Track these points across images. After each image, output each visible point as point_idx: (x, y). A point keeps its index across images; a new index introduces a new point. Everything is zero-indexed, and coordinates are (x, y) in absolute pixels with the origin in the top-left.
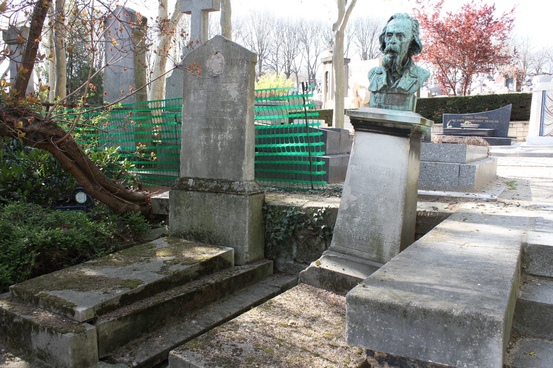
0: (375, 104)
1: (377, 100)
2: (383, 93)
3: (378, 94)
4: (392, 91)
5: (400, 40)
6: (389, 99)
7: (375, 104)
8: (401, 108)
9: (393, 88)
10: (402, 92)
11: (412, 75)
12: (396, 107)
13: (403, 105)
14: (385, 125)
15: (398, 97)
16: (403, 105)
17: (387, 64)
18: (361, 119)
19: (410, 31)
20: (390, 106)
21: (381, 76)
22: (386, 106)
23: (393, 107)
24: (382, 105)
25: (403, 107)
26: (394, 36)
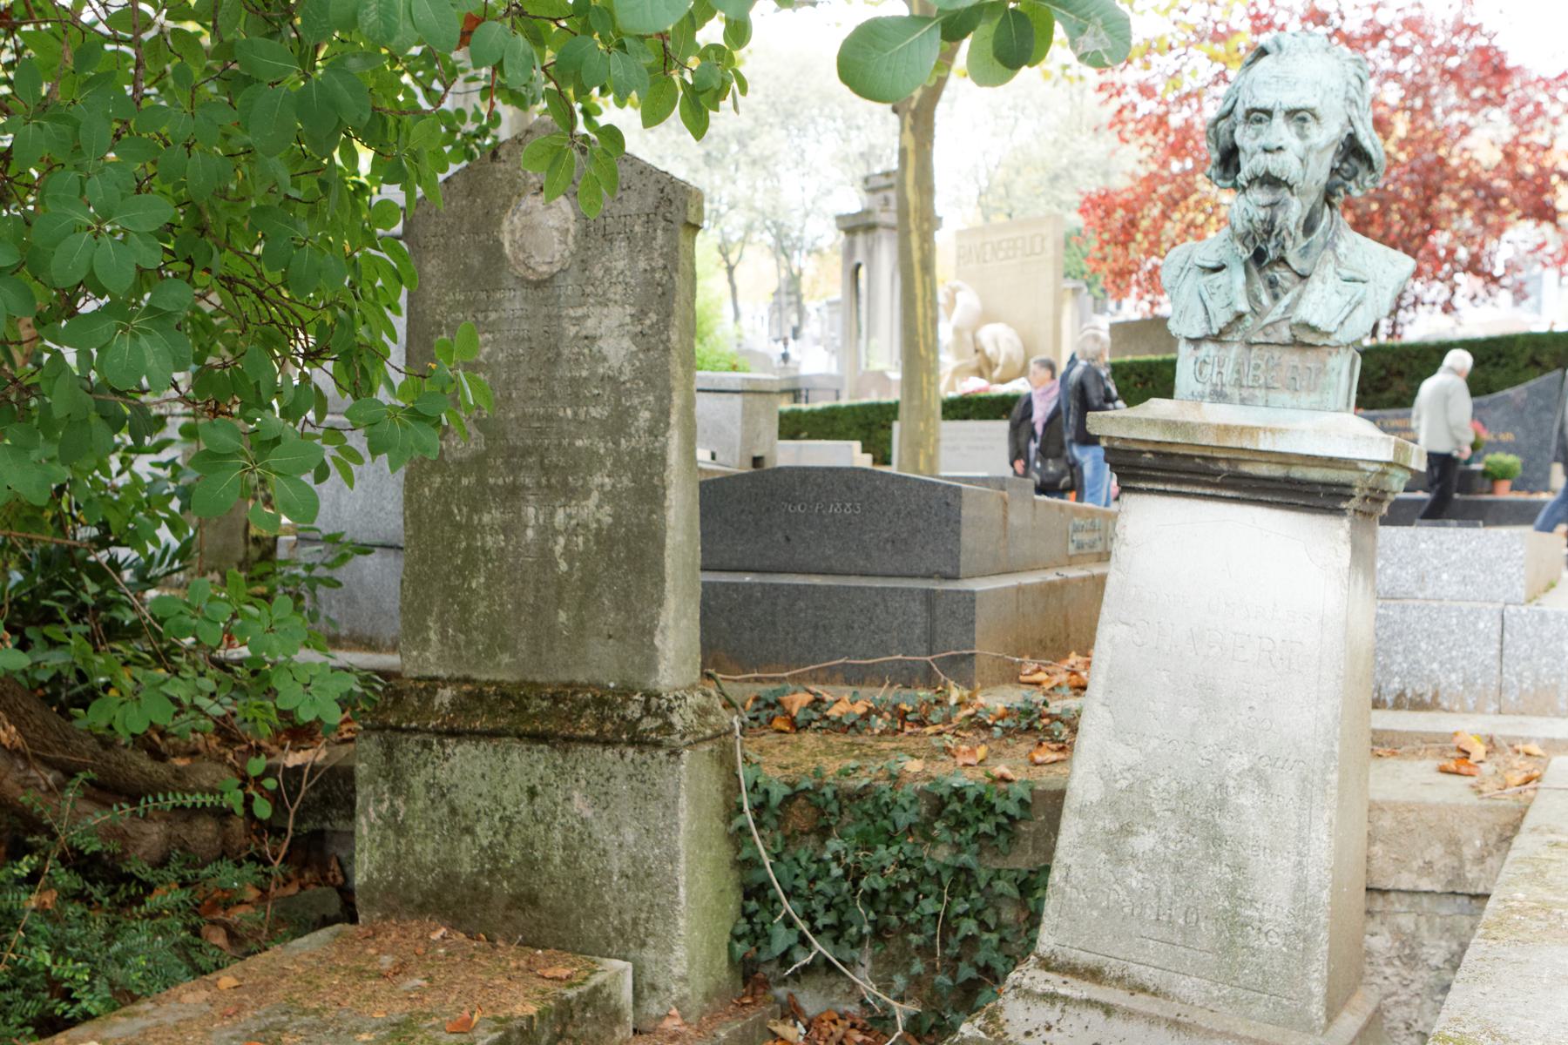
0: (1199, 387)
1: (1207, 370)
2: (1232, 342)
3: (1209, 349)
4: (1266, 335)
5: (1302, 136)
6: (1257, 367)
7: (1199, 387)
8: (1306, 399)
9: (1271, 324)
10: (1309, 338)
11: (1347, 274)
12: (1285, 397)
13: (1314, 390)
14: (1246, 469)
15: (1292, 358)
16: (1311, 389)
17: (1249, 233)
18: (1151, 447)
19: (1338, 103)
20: (1260, 393)
21: (1220, 278)
22: (1245, 393)
23: (1273, 395)
24: (1228, 390)
25: (1314, 397)
26: (1278, 120)
